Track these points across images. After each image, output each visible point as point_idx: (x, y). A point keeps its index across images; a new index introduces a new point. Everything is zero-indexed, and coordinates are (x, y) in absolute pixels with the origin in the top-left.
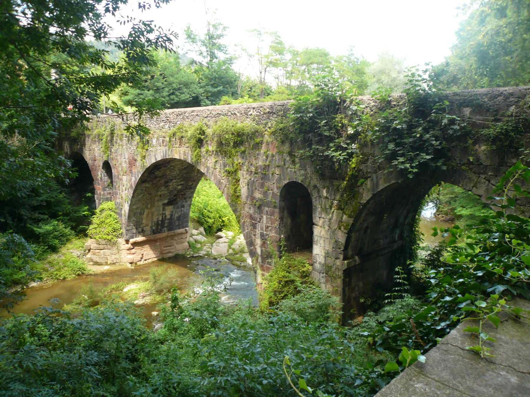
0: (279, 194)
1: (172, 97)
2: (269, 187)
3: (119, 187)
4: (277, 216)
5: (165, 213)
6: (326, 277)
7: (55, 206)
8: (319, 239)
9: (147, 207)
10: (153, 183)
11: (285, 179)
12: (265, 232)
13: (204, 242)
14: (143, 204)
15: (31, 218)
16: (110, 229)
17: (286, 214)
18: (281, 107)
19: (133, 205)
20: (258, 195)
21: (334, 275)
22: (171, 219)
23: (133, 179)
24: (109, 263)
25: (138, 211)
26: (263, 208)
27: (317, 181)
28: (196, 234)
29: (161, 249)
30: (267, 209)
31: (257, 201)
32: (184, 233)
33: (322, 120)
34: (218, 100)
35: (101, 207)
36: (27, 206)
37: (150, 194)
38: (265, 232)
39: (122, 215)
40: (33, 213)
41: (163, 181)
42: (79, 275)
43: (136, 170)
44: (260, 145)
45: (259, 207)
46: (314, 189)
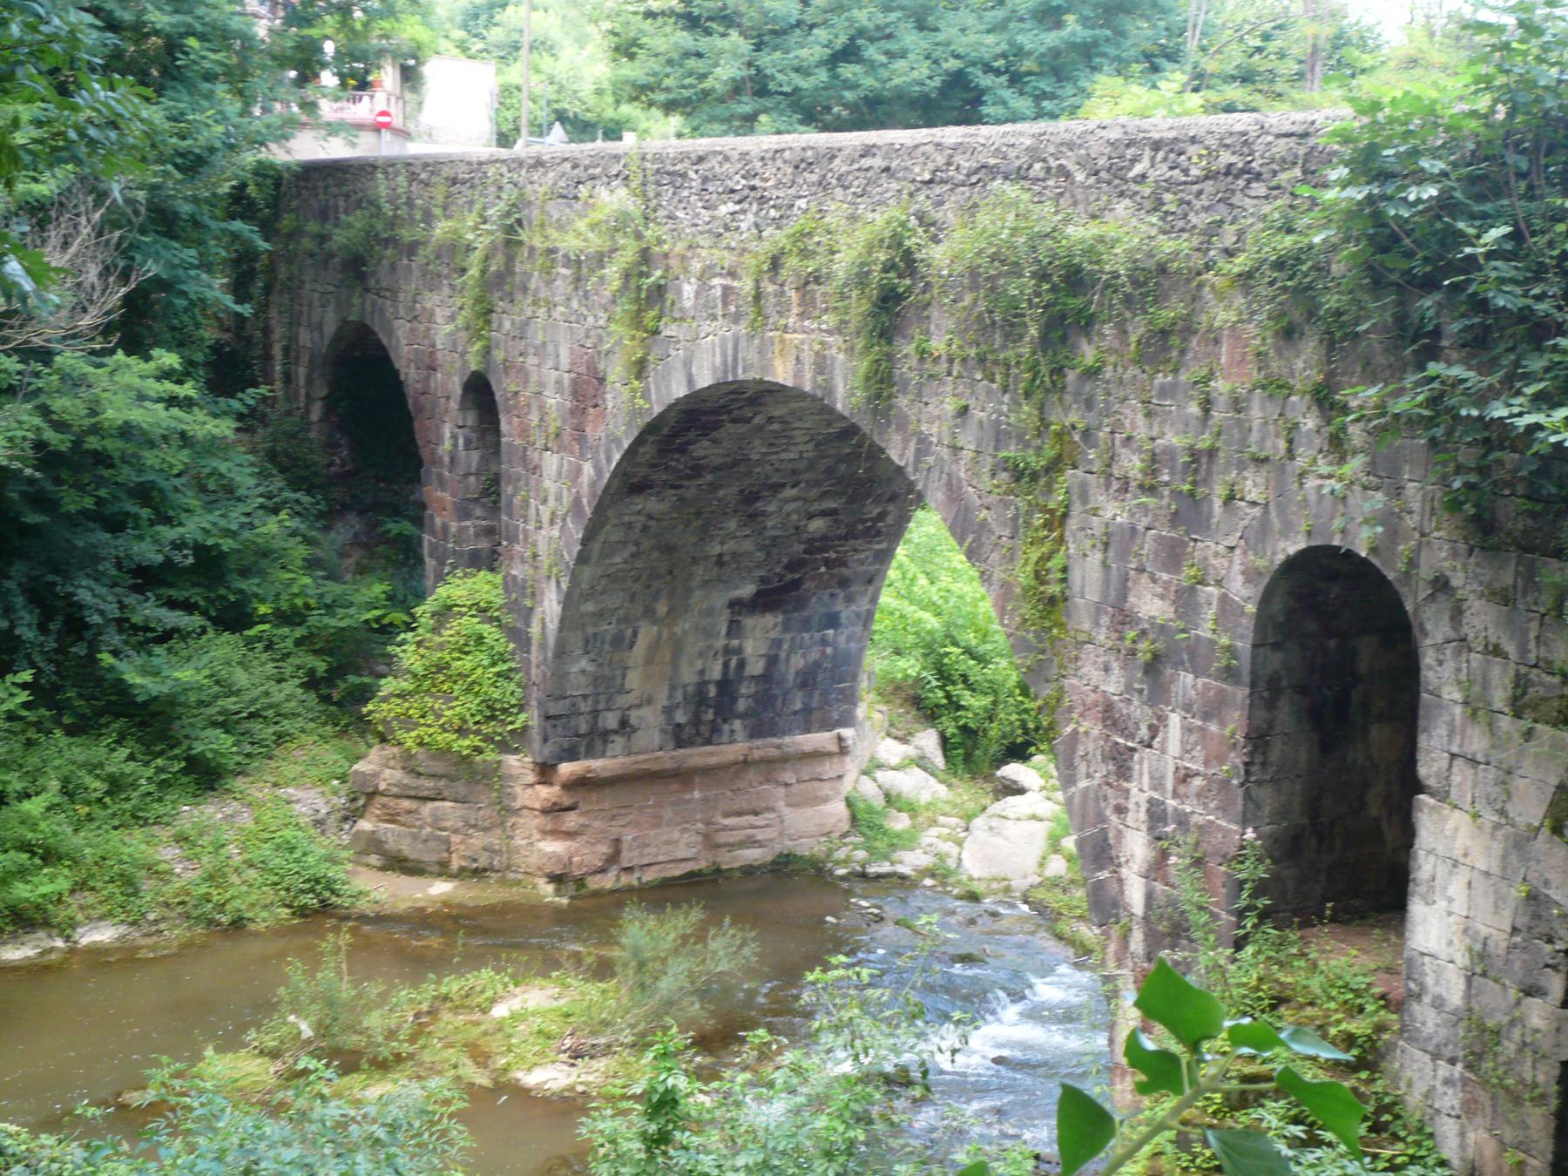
0: (1251, 608)
1: (847, 71)
2: (1204, 566)
3: (526, 503)
4: (1234, 723)
5: (739, 650)
6: (1465, 1082)
7: (245, 573)
8: (1442, 871)
9: (649, 613)
10: (682, 499)
11: (1287, 530)
12: (1171, 803)
13: (928, 806)
14: (633, 598)
15: (122, 624)
16: (474, 704)
17: (1285, 715)
18: (1292, 141)
19: (585, 598)
20: (1151, 605)
21: (1510, 1081)
22: (766, 678)
23: (588, 469)
24: (456, 864)
25: (608, 628)
26: (1169, 671)
27: (1454, 554)
28: (895, 761)
29: (708, 823)
30: (1188, 678)
31: (1144, 633)
32: (829, 755)
33: (1487, 221)
34: (1069, 89)
35: (442, 591)
36: (108, 567)
37: (669, 550)
38: (1171, 803)
39: (528, 641)
40: (132, 599)
41: (734, 490)
42: (302, 912)
43: (601, 432)
44: (1175, 341)
45: (1153, 667)
46: (1432, 598)
